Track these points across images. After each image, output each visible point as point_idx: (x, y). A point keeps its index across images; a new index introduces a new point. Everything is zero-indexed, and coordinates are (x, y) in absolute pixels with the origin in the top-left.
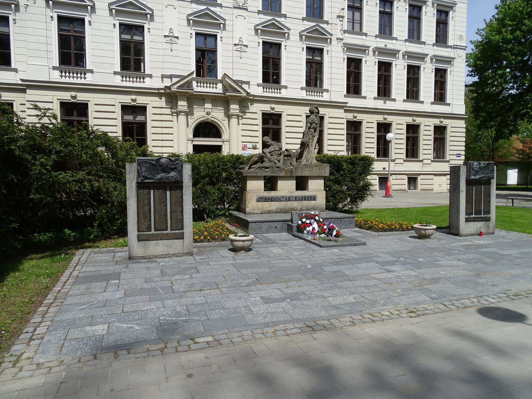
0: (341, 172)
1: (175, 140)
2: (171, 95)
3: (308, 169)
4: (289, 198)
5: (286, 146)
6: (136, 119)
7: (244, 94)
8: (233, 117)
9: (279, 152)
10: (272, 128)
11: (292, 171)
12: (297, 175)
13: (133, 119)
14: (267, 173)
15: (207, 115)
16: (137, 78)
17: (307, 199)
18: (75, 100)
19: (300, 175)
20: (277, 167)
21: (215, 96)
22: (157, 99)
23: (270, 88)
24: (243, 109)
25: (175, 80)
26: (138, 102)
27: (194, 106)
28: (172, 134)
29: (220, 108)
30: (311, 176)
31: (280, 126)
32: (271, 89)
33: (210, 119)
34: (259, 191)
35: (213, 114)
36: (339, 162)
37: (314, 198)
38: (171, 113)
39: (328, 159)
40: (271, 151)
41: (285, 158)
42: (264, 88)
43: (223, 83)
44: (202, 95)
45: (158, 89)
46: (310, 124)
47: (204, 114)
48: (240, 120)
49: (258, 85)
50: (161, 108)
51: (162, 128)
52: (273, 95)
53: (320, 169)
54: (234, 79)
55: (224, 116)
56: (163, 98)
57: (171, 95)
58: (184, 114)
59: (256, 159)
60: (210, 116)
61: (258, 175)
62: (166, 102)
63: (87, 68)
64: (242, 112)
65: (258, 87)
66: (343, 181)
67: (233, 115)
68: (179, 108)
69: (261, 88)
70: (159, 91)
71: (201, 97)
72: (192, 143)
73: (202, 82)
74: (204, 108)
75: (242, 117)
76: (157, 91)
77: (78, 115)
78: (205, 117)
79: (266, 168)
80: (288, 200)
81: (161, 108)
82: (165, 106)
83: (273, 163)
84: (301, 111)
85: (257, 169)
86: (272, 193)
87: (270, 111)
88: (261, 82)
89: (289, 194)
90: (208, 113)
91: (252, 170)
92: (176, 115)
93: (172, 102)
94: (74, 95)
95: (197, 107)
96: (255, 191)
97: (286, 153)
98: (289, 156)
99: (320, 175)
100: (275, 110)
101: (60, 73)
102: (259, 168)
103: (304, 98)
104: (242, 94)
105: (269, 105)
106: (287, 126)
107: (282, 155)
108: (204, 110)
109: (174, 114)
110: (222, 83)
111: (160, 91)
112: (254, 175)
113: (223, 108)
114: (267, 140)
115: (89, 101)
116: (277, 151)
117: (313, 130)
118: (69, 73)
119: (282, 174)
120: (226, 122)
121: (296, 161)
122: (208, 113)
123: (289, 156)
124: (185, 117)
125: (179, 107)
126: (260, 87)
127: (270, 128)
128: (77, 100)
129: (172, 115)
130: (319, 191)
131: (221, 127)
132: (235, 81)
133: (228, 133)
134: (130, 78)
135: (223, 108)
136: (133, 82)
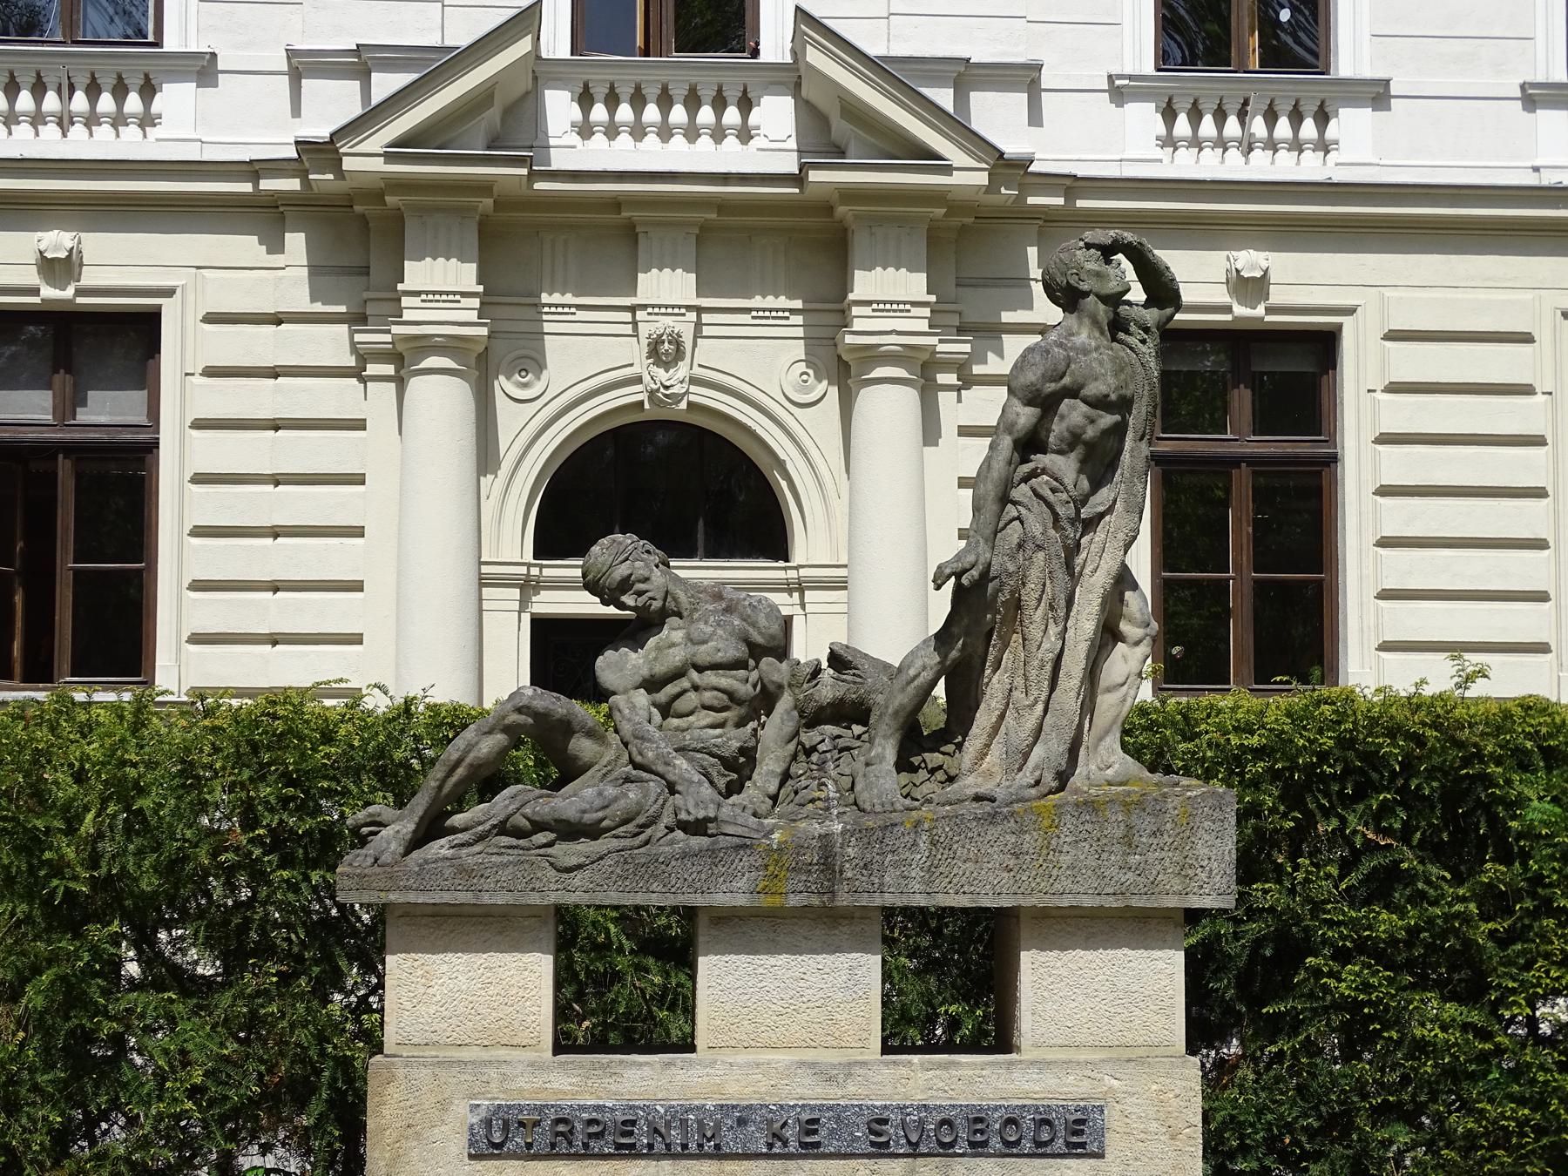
0: (1492, 871)
1: (380, 585)
2: (358, 208)
3: (1001, 837)
4: (811, 1126)
5: (1378, 613)
6: (83, 416)
7: (968, 175)
8: (880, 372)
9: (741, 684)
10: (1252, 461)
11: (828, 863)
12: (889, 900)
13: (48, 417)
14: (578, 879)
15: (659, 362)
16: (93, 91)
17: (996, 1143)
18: (1260, 311)
19: (920, 901)
20: (685, 827)
21: (723, 206)
22: (245, 247)
23: (1232, 106)
24: (974, 305)
25: (385, 84)
26: (89, 278)
27: (545, 298)
28: (358, 532)
29: (770, 301)
30: (411, 913)
31: (1332, 440)
32: (1242, 116)
33: (678, 398)
34: (503, 1053)
35: (711, 355)
36: (1466, 762)
37: (1078, 1126)
38: (351, 361)
39: (1341, 742)
40: (660, 669)
41: (809, 737)
42: (1169, 115)
43: (805, 92)
44: (616, 203)
45: (254, 170)
46: (1029, 403)
47: (633, 354)
48: (946, 400)
49: (1120, 91)
50: (277, 319)
51: (277, 480)
52: (1262, 167)
53: (1128, 841)
54: (873, 50)
55: (802, 367)
56: (296, 242)
57: (358, 208)
58: (900, 372)
59: (488, 746)
60: (682, 370)
61: (486, 899)
62: (315, 270)
63: (171, 44)
64: (961, 330)
65: (1120, 105)
66: (1509, 962)
67: (873, 356)
68: (407, 315)
69: (1144, 117)
70: (256, 185)
71: (608, 217)
72: (524, 603)
73: (625, 91)
74: (632, 309)
75: (961, 368)
76: (247, 187)
77: (1263, 424)
78: (638, 380)
79: (570, 831)
80: (793, 1147)
81: (277, 319)
82: (304, 304)
83: (655, 786)
84: (1529, 295)
85: (481, 838)
86: (632, 1074)
87: (1227, 309)
88: (1148, 68)
89: (806, 1091)
90: (664, 352)
91: (439, 848)
92: (389, 369)
93: (365, 271)
94: (63, 255)
95: (569, 298)
96: (465, 1054)
97: (829, 688)
98: (852, 712)
99: (1136, 902)
100: (1277, 296)
101: (576, 106)
102: (503, 829)
103: (1548, 179)
104: (948, 170)
105: (1220, 256)
106: (1385, 439)
107: (785, 703)
108: (635, 323)
109: (372, 369)
110: (796, 90)
111: (266, 184)
112: (446, 897)
113: (798, 304)
114: (622, 571)
115: (169, 292)
116: (715, 667)
117: (1066, 466)
118: (659, 103)
119: (733, 892)
120: (822, 422)
121: (903, 765)
122: (664, 352)
123: (852, 712)
124: (908, 398)
125: (412, 309)
126: (1132, 107)
127: (1235, 461)
128: (1269, 310)
129: (357, 373)
130: (1131, 1057)
131: (781, 465)
132: (882, 70)
133: (840, 507)
134: (39, 90)
135: (798, 304)
136: (64, 122)
